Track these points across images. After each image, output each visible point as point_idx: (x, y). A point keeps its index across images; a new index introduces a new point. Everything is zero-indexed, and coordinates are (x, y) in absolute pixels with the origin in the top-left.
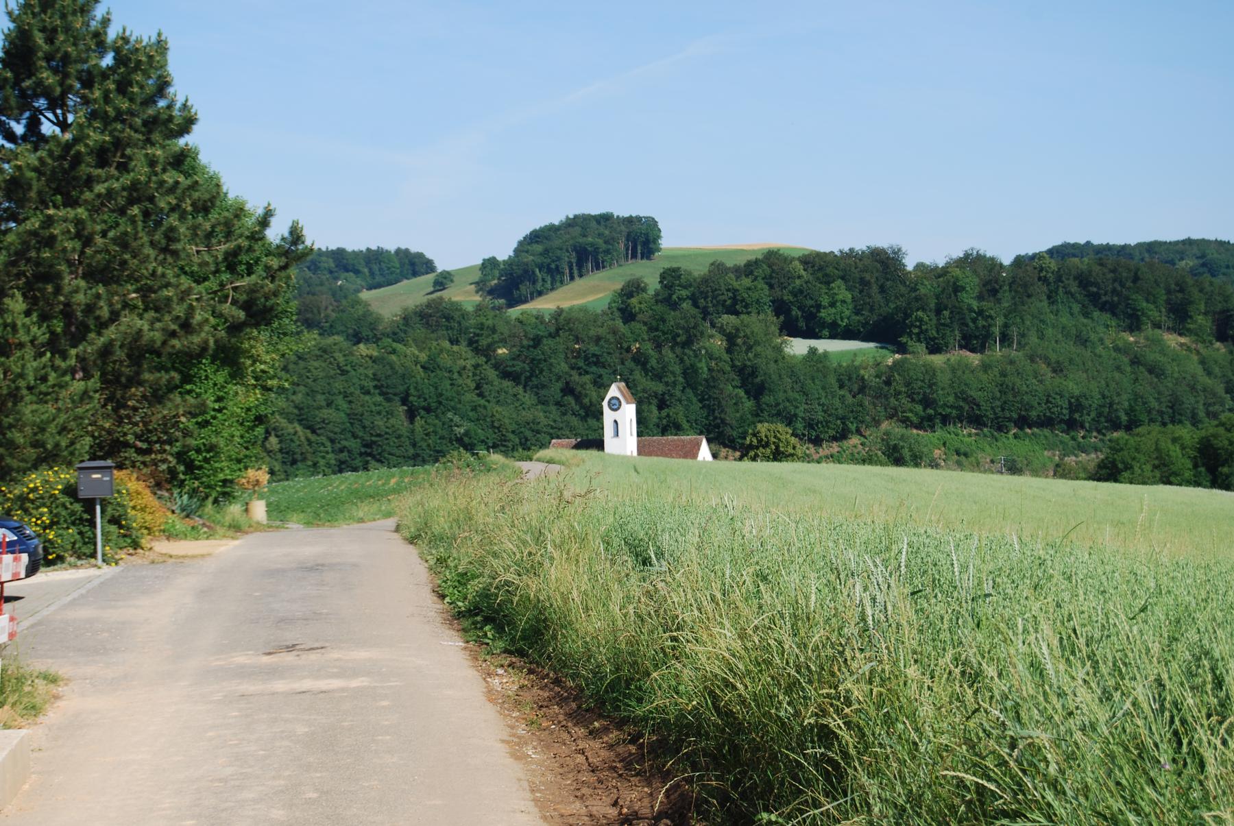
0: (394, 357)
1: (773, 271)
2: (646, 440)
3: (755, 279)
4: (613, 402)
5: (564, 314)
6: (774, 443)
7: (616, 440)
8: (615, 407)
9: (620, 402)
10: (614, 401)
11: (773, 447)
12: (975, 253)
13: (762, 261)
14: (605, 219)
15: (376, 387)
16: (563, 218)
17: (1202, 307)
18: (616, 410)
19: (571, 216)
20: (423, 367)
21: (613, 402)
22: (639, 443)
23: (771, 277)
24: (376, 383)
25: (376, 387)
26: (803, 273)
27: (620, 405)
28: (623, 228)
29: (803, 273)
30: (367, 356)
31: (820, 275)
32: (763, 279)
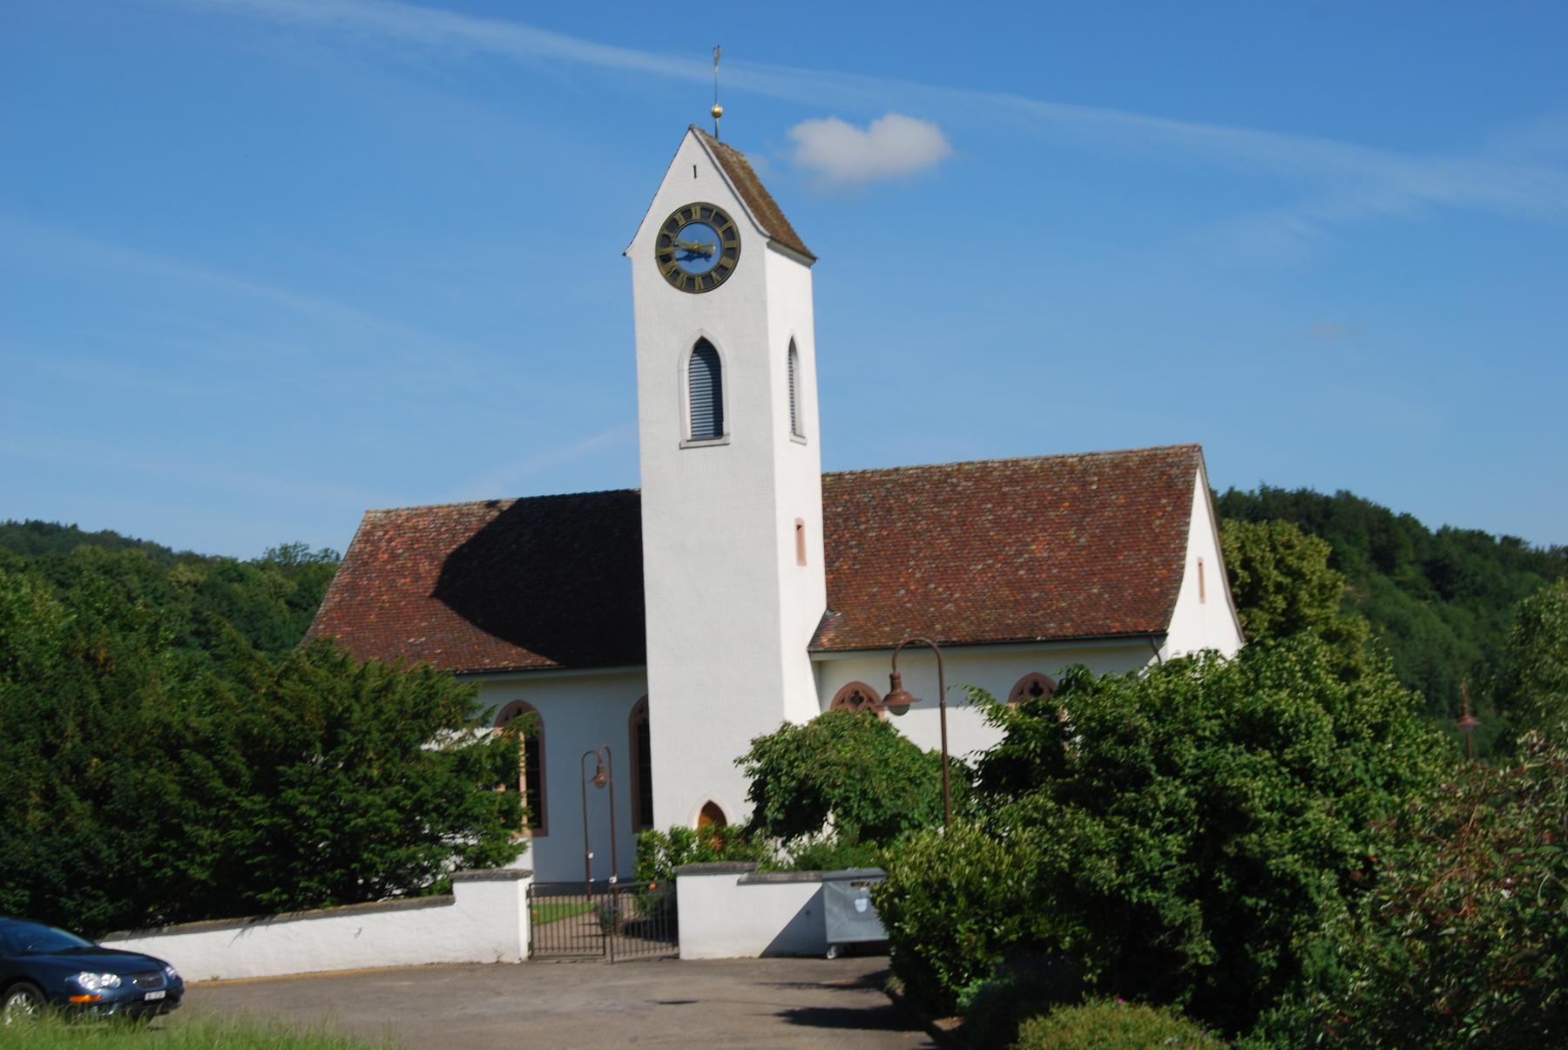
0: (237, 587)
6: (1279, 588)
7: (708, 456)
8: (699, 267)
9: (731, 234)
10: (698, 235)
11: (1280, 603)
15: (196, 633)
17: (1412, 556)
18: (710, 282)
20: (289, 603)
24: (194, 626)
25: (196, 633)
27: (732, 252)
30: (189, 582)
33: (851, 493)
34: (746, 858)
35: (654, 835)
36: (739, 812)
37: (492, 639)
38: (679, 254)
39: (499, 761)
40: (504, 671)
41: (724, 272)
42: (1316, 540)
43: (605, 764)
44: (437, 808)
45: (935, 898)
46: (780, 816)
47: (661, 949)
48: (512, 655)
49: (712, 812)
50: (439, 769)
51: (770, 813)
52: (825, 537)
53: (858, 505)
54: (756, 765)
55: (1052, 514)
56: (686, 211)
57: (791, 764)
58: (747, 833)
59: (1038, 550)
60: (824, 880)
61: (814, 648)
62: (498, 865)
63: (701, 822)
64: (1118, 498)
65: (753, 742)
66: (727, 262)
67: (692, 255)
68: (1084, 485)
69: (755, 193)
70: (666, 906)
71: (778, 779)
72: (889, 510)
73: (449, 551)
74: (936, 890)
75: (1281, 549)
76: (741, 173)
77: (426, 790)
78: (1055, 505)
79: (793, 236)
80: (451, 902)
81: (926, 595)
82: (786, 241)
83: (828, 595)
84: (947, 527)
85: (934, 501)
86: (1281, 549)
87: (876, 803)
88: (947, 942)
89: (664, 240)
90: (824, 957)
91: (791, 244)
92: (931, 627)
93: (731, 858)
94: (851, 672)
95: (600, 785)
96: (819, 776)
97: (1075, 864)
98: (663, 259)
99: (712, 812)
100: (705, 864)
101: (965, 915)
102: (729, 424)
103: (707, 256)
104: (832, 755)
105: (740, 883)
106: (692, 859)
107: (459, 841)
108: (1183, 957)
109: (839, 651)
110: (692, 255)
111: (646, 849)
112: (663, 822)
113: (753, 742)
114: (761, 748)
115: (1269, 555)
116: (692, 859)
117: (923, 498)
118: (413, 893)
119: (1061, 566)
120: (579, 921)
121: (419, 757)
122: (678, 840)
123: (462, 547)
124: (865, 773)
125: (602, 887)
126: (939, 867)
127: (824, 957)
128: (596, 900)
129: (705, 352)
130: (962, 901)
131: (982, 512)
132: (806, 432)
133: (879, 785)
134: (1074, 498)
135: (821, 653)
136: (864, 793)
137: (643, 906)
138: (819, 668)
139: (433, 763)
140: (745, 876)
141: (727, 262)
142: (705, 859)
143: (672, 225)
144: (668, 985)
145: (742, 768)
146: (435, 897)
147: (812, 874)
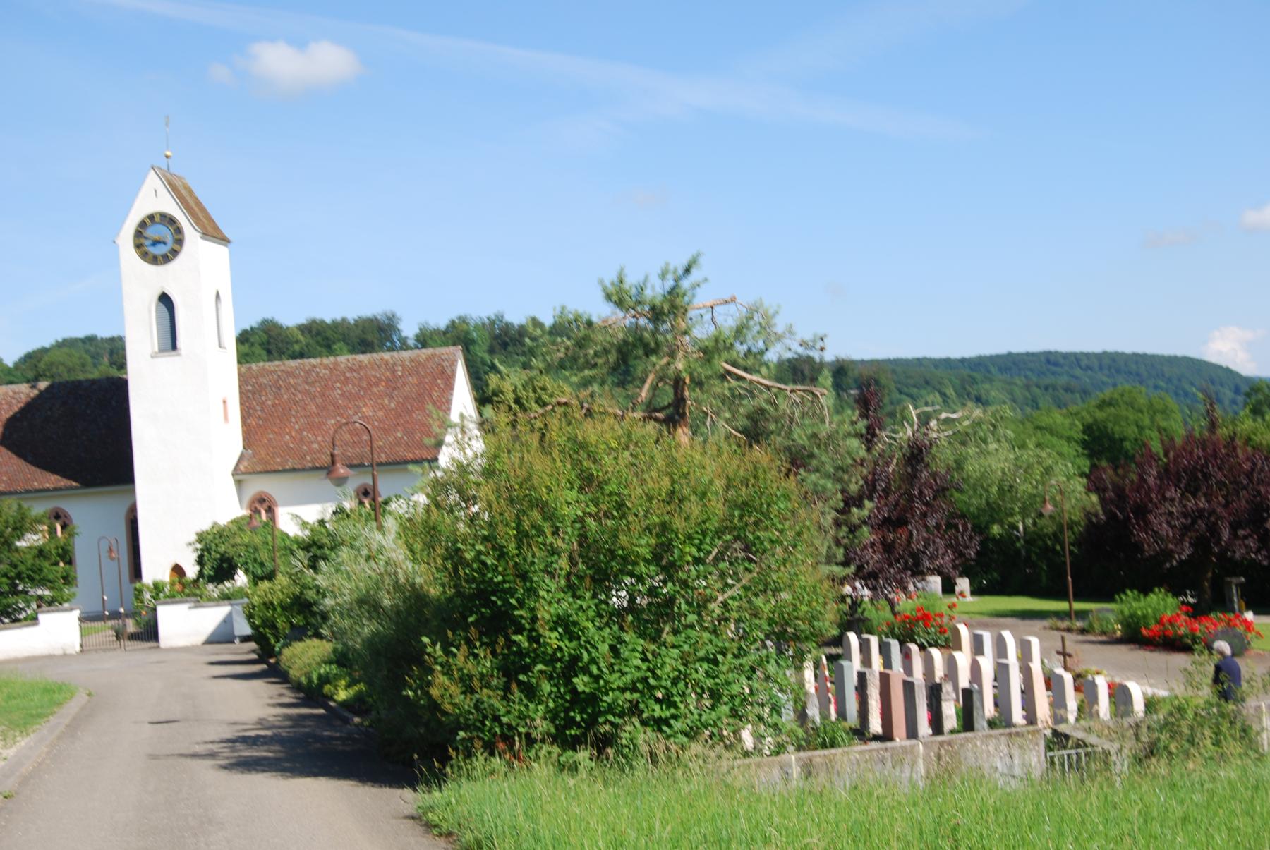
1: (270, 336)
2: (263, 372)
3: (252, 345)
4: (154, 232)
5: (46, 358)
7: (168, 361)
8: (160, 250)
9: (179, 231)
12: (486, 321)
13: (258, 329)
14: (91, 340)
16: (53, 342)
18: (165, 260)
19: (60, 340)
21: (154, 232)
22: (243, 380)
23: (269, 343)
26: (301, 338)
27: (180, 242)
28: (106, 345)
29: (301, 338)
31: (319, 338)
32: (260, 345)
33: (257, 378)
34: (196, 595)
35: (143, 585)
36: (192, 571)
37: (38, 470)
38: (147, 242)
39: (60, 551)
40: (48, 490)
41: (175, 253)
42: (561, 384)
43: (114, 548)
44: (29, 577)
45: (268, 608)
46: (212, 573)
47: (152, 644)
48: (52, 480)
49: (178, 570)
50: (28, 556)
51: (207, 572)
52: (241, 404)
53: (260, 385)
54: (199, 546)
55: (375, 390)
56: (151, 217)
57: (217, 545)
58: (196, 581)
59: (367, 411)
60: (231, 605)
61: (236, 472)
62: (61, 604)
63: (171, 575)
64: (413, 380)
65: (197, 534)
66: (176, 247)
67: (156, 243)
68: (394, 372)
69: (192, 203)
70: (152, 623)
71: (210, 554)
72: (279, 388)
73: (8, 416)
74: (268, 605)
75: (539, 390)
76: (184, 192)
77: (22, 568)
78: (377, 384)
79: (216, 228)
80: (37, 624)
81: (301, 440)
82: (212, 233)
83: (244, 440)
84: (313, 398)
85: (307, 383)
86: (539, 390)
87: (262, 565)
88: (273, 626)
89: (139, 234)
90: (234, 642)
91: (215, 234)
92: (303, 458)
93: (188, 595)
94: (259, 485)
95: (112, 559)
96: (231, 552)
97: (301, 593)
98: (138, 246)
99: (178, 570)
100: (172, 599)
101: (280, 615)
102: (180, 343)
103: (165, 243)
104: (238, 540)
105: (190, 608)
106: (166, 596)
107: (40, 592)
108: (299, 613)
109: (250, 473)
110: (156, 243)
111: (139, 593)
112: (149, 576)
113: (197, 534)
114: (201, 537)
115: (531, 394)
116: (166, 596)
117: (299, 381)
118: (16, 620)
119: (380, 421)
120: (105, 631)
121: (17, 549)
122: (157, 588)
123: (16, 413)
124: (256, 549)
125: (115, 615)
126: (269, 596)
127: (234, 642)
128: (110, 623)
129: (165, 300)
130: (279, 610)
131: (333, 388)
132: (226, 346)
133: (264, 556)
134: (388, 380)
135: (240, 475)
136: (255, 560)
137: (138, 623)
138: (239, 483)
139: (24, 553)
140: (192, 604)
141: (176, 247)
142: (173, 596)
143: (143, 224)
144: (154, 656)
145: (191, 548)
146: (29, 622)
147: (226, 602)
